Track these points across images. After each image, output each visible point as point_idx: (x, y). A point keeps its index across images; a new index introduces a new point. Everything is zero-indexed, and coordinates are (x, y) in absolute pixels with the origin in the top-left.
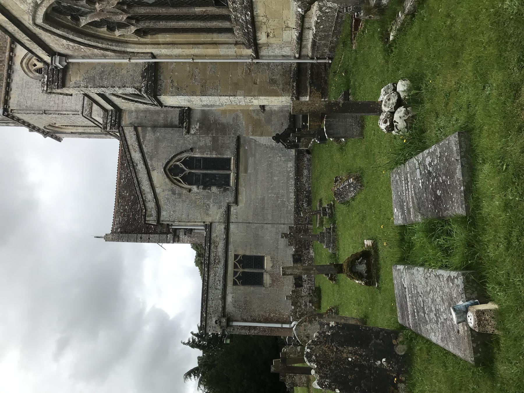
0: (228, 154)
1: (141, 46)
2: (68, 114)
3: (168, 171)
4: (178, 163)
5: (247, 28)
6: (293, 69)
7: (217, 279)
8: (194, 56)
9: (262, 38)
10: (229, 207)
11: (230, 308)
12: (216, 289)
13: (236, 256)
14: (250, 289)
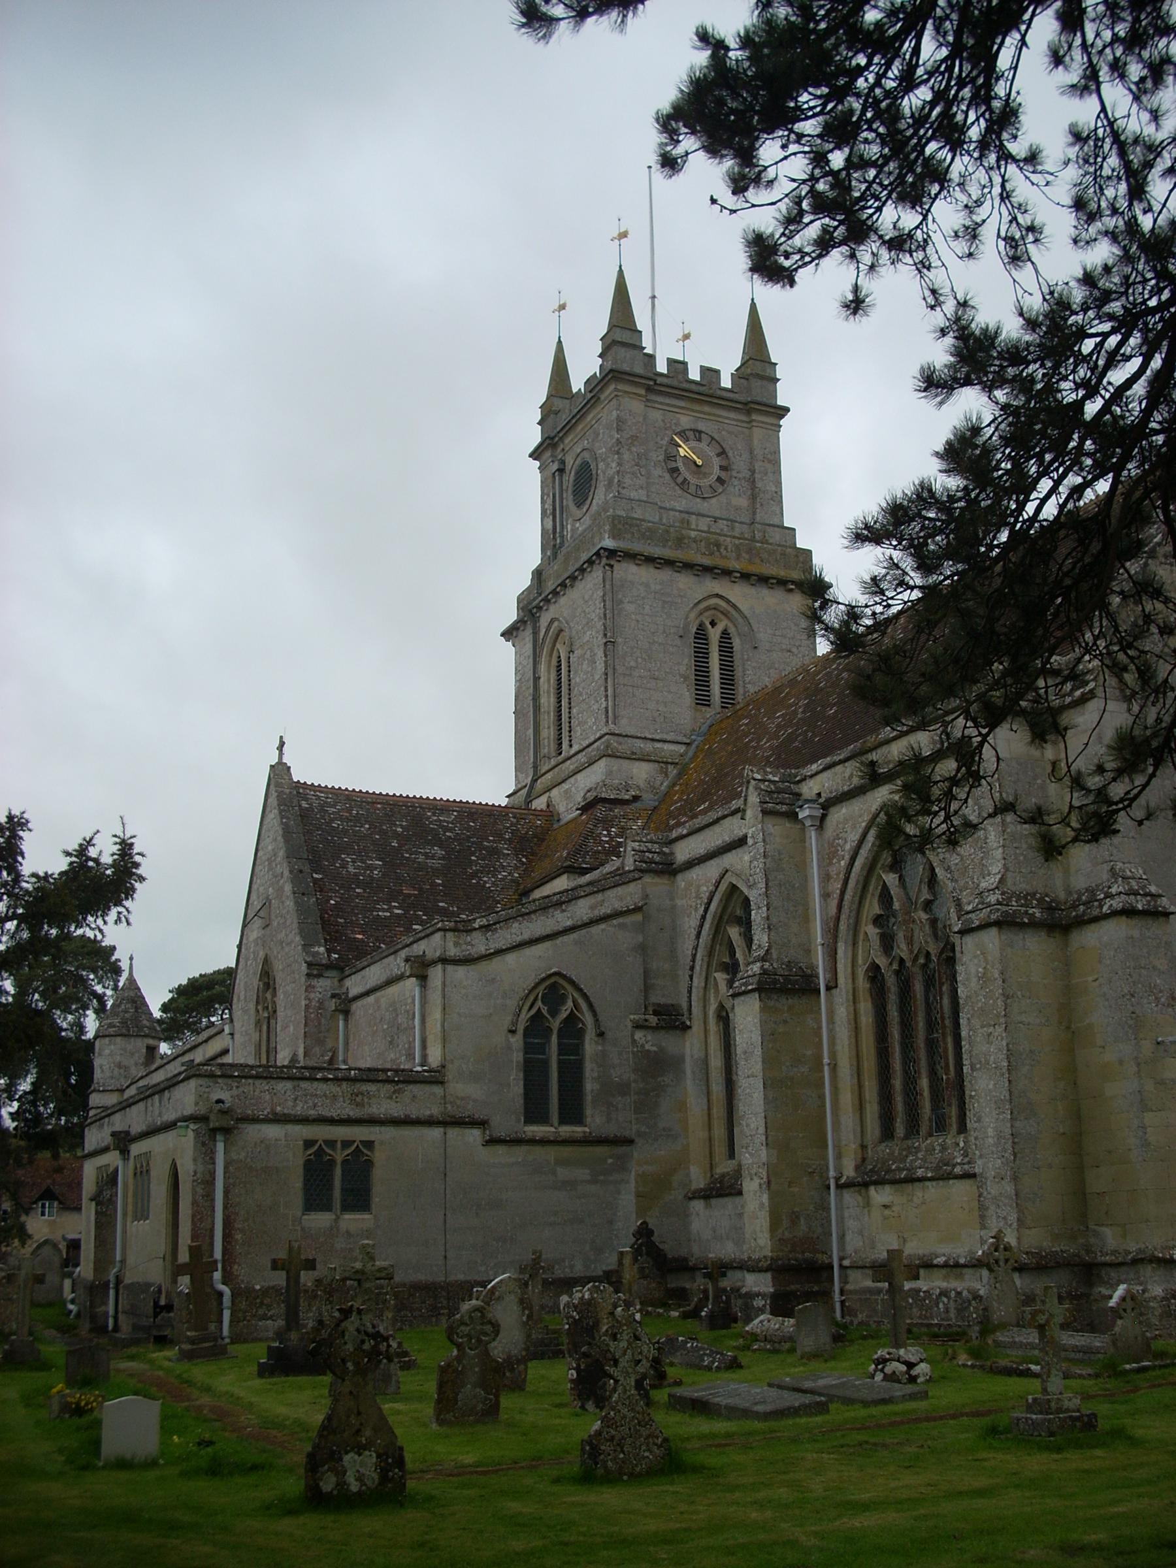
0: (595, 1121)
1: (849, 970)
2: (607, 696)
3: (552, 980)
4: (570, 1004)
5: (899, 1169)
6: (819, 1256)
8: (834, 1068)
9: (880, 1196)
10: (482, 1124)
11: (252, 1132)
12: (296, 1099)
13: (369, 1144)
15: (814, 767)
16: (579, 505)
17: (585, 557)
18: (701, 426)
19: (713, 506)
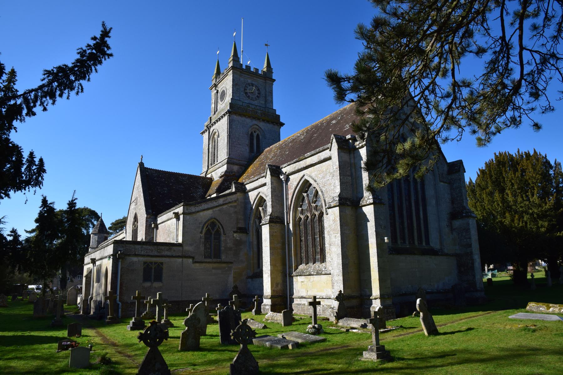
3: (212, 221)
7: (148, 251)
13: (162, 263)
14: (141, 274)
15: (285, 165)
16: (221, 101)
17: (223, 113)
18: (253, 83)
19: (256, 103)
